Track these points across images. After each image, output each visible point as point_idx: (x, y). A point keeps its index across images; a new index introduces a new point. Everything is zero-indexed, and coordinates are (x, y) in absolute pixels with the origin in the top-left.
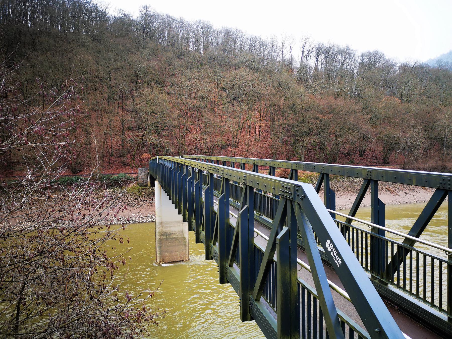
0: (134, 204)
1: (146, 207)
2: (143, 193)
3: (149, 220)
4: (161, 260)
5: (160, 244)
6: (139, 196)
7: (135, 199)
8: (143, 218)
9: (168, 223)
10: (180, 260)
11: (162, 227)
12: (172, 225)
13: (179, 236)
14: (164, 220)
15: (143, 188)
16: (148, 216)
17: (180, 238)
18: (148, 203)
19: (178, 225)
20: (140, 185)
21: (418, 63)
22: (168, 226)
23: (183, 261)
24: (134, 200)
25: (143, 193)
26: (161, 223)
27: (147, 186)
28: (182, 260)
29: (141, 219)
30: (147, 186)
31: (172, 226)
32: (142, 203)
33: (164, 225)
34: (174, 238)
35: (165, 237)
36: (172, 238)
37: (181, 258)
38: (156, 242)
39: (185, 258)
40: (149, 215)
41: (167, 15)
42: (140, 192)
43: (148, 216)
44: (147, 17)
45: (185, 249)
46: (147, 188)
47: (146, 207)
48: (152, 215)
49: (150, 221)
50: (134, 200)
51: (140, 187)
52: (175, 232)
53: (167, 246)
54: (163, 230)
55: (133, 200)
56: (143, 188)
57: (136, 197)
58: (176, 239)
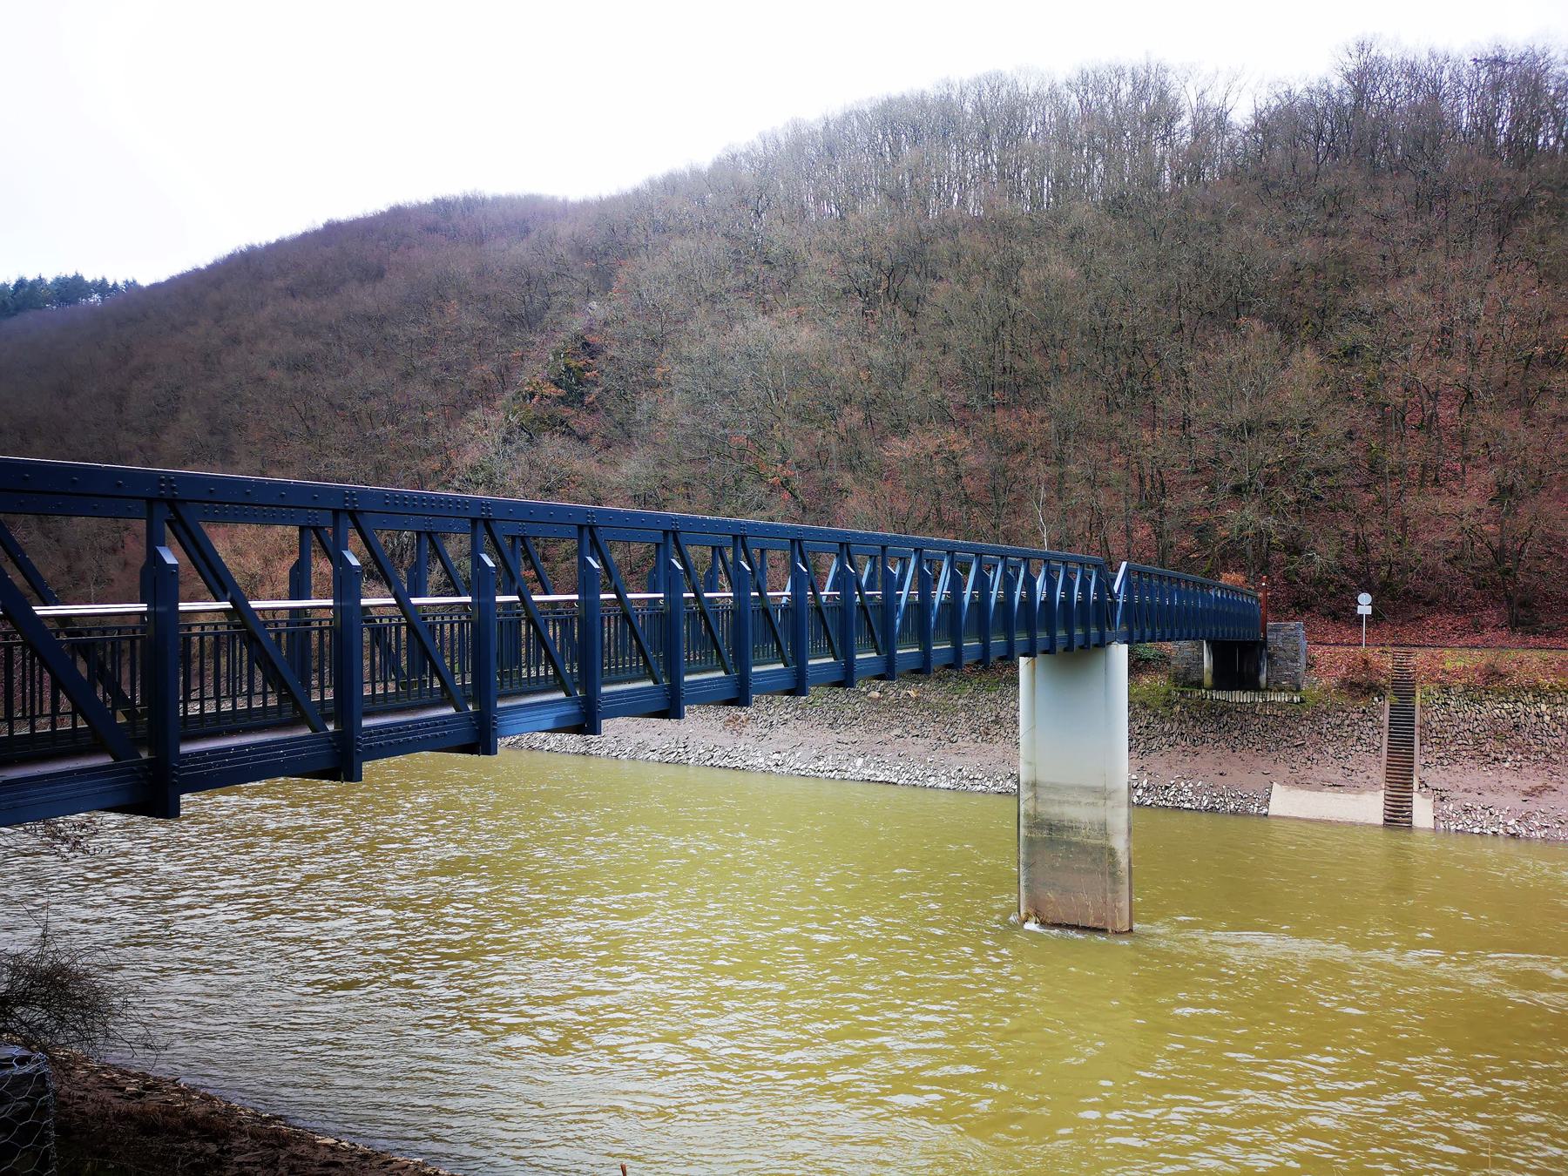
0: (1134, 741)
1: (1175, 755)
2: (1177, 708)
3: (1166, 799)
4: (1031, 911)
5: (1028, 854)
6: (1162, 717)
7: (1144, 724)
8: (1147, 790)
9: (1055, 788)
10: (1095, 925)
11: (1036, 798)
12: (1070, 799)
13: (1093, 841)
14: (1044, 777)
15: (1182, 692)
16: (1167, 788)
17: (1094, 847)
18: (1183, 743)
19: (1090, 800)
20: (1176, 680)
21: (782, 140)
22: (1056, 798)
23: (1103, 931)
24: (1140, 727)
25: (1177, 708)
26: (1034, 785)
27: (1199, 685)
28: (1100, 925)
29: (1140, 792)
30: (1199, 685)
31: (1068, 802)
32: (1164, 740)
33: (1044, 795)
34: (1076, 844)
35: (1045, 834)
36: (1069, 844)
37: (1098, 919)
38: (1019, 846)
39: (1114, 923)
40: (1172, 782)
41: (1430, 53)
42: (1168, 704)
43: (1167, 788)
44: (1363, 79)
45: (1115, 892)
46: (1198, 693)
47: (1174, 755)
48: (1182, 784)
49: (1169, 804)
50: (1140, 727)
51: (1176, 686)
52: (1078, 825)
53: (1053, 868)
54: (1040, 809)
55: (1137, 727)
56: (1182, 692)
57: (1152, 718)
58: (1083, 849)
